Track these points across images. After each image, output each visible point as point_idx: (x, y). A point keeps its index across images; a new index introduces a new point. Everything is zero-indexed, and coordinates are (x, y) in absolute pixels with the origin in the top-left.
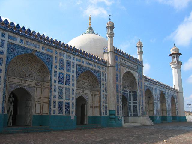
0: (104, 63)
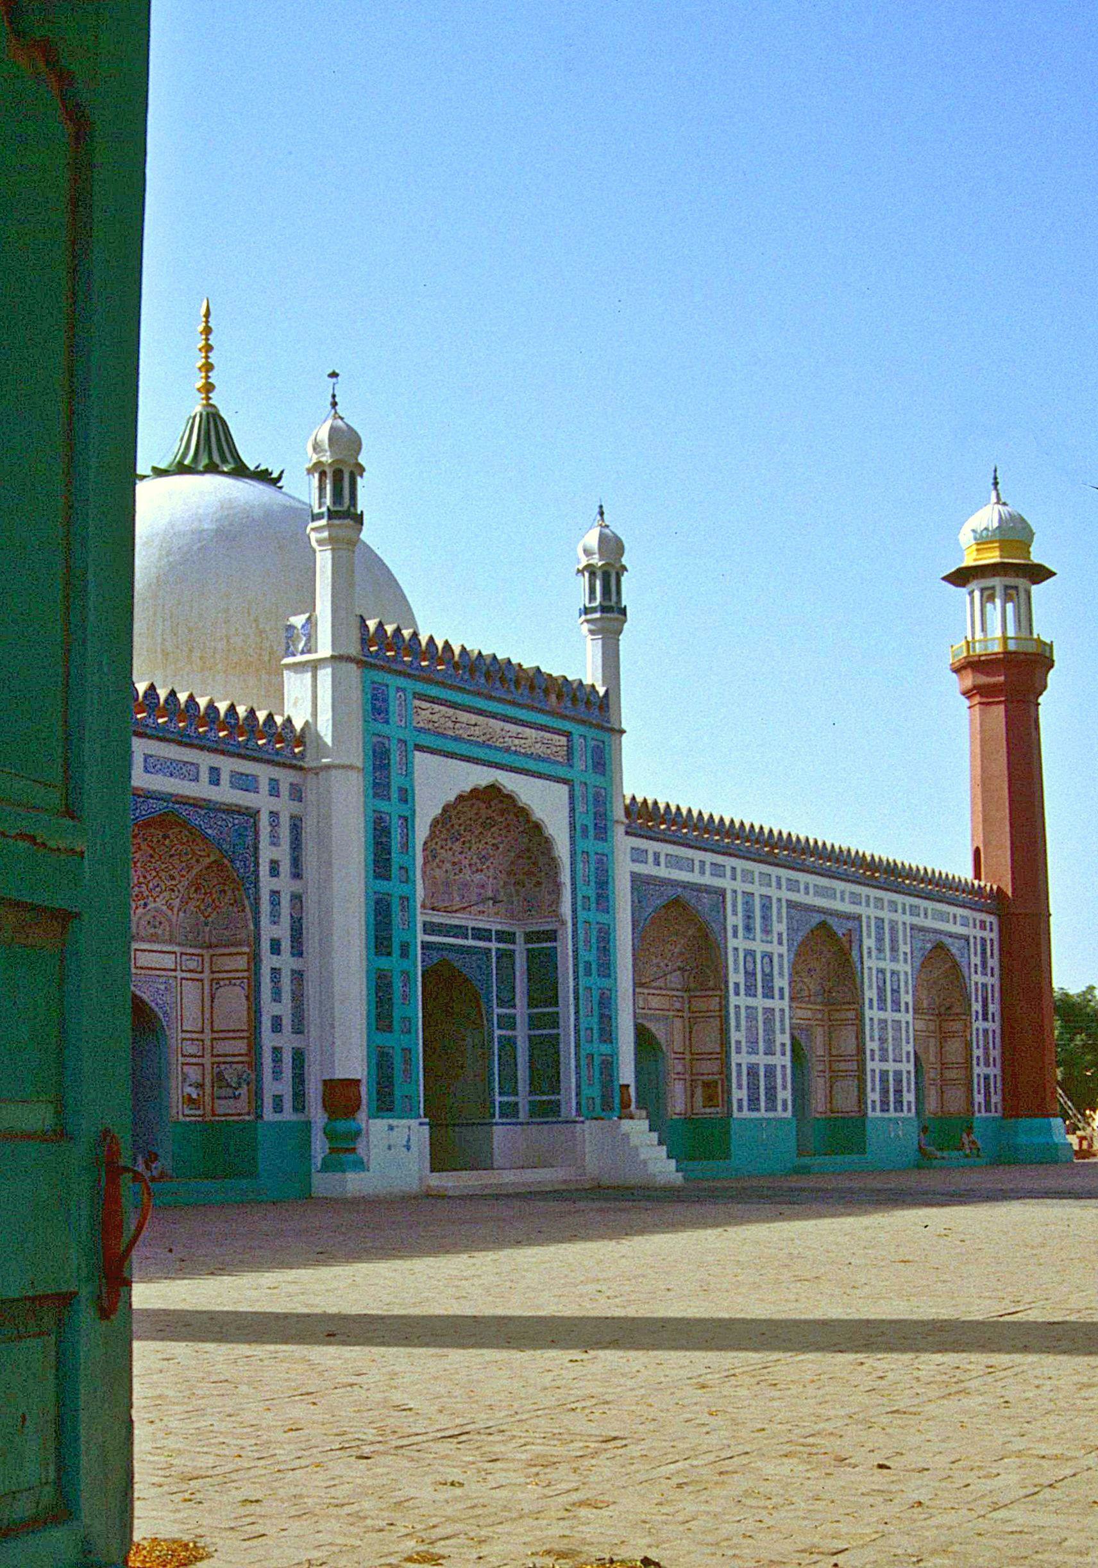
0: (283, 745)
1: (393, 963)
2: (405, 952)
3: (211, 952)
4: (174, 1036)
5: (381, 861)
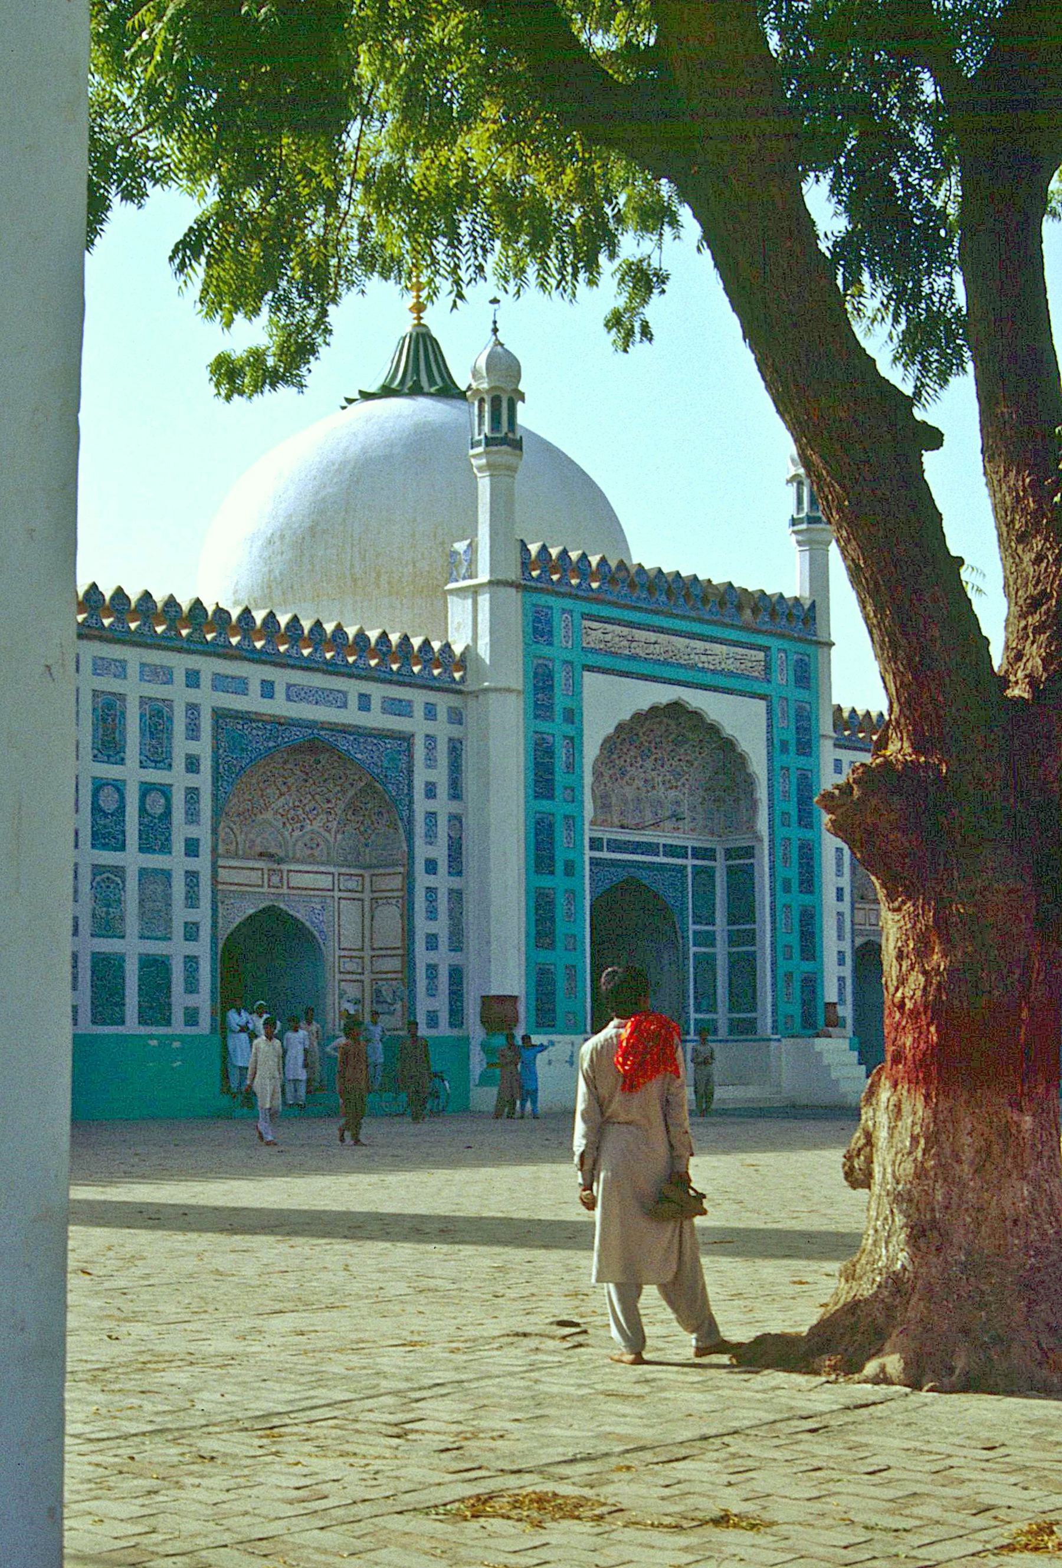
0: (440, 671)
2: (570, 869)
3: (372, 871)
4: (331, 953)
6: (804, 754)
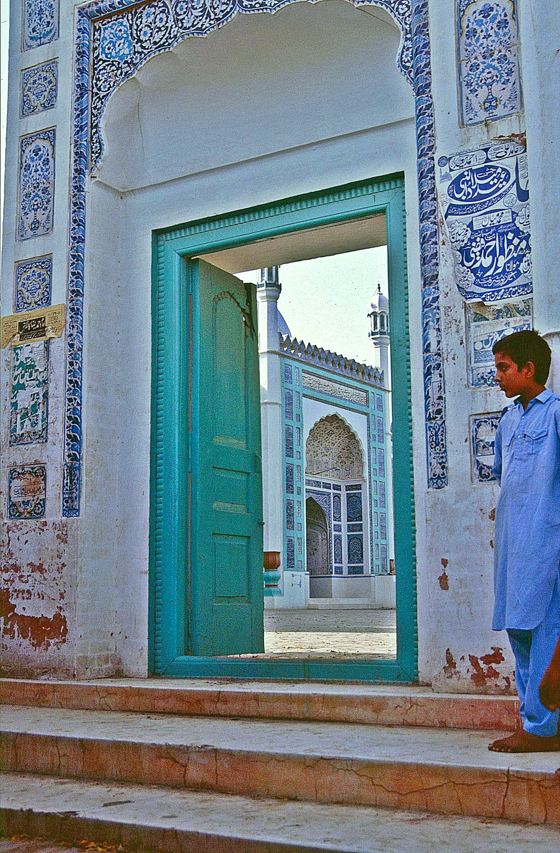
1: (294, 497)
5: (289, 450)
6: (290, 456)
